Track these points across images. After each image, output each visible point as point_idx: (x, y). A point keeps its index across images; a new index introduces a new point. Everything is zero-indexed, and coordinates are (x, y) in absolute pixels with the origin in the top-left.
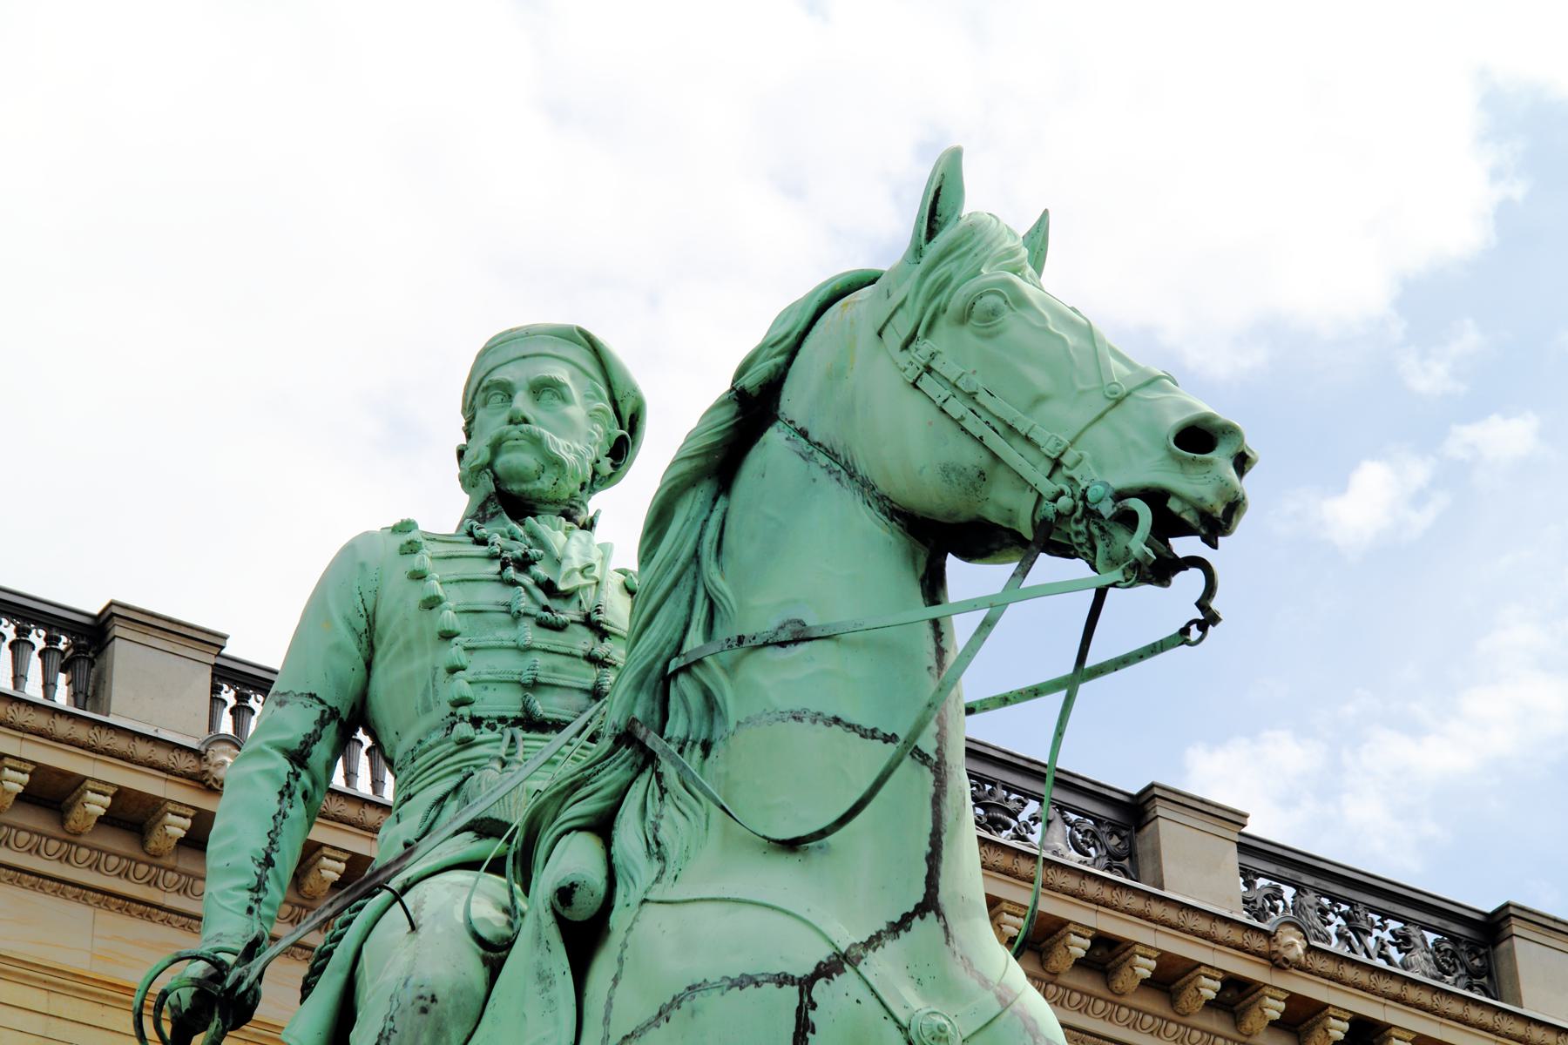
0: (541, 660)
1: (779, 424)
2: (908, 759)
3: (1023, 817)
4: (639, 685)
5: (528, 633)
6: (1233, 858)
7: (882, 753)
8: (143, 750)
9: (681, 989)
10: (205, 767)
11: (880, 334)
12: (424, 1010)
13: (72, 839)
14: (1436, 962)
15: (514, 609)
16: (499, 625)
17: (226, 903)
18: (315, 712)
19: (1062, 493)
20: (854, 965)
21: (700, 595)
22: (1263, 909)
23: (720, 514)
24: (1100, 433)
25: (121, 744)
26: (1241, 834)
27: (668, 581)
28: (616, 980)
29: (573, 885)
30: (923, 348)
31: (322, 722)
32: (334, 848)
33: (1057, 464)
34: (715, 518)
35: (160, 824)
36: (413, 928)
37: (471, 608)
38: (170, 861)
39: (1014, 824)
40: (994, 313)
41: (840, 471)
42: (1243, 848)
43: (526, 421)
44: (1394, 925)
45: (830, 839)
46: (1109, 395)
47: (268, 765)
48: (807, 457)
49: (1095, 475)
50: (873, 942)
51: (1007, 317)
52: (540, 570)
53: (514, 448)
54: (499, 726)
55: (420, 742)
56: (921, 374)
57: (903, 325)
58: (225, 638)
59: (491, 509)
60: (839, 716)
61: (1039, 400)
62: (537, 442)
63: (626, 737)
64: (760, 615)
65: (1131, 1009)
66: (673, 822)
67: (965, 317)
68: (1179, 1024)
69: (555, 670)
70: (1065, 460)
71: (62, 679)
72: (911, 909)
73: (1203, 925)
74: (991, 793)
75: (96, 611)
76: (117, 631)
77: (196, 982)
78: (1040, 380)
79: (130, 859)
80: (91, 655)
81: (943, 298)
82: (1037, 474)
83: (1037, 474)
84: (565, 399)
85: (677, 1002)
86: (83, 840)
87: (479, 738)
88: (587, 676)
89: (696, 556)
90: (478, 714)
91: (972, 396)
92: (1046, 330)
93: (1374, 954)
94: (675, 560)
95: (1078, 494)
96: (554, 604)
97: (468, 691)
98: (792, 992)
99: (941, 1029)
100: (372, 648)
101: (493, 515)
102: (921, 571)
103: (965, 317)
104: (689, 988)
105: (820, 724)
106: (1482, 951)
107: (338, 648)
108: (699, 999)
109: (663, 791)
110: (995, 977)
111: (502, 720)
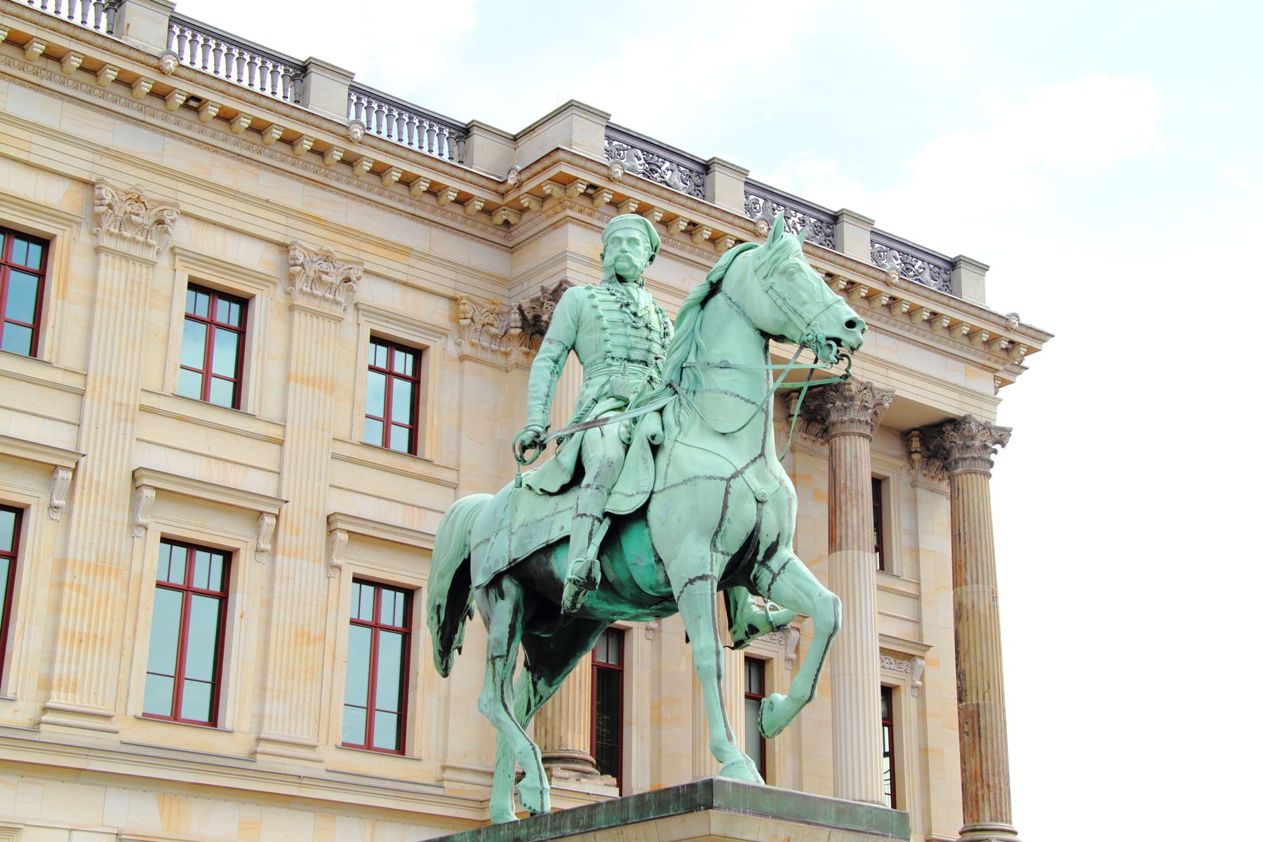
0: (632, 339)
1: (722, 293)
3: (663, 168)
4: (674, 369)
5: (630, 331)
6: (742, 187)
8: (326, 125)
9: (692, 477)
10: (349, 133)
12: (610, 466)
13: (297, 157)
14: (814, 232)
15: (625, 322)
16: (620, 326)
17: (537, 409)
18: (561, 347)
19: (809, 334)
20: (742, 474)
21: (694, 343)
22: (751, 208)
24: (822, 317)
25: (317, 122)
26: (747, 178)
27: (684, 337)
28: (668, 465)
29: (656, 435)
30: (771, 280)
32: (397, 168)
35: (331, 154)
36: (602, 435)
38: (333, 168)
39: (660, 171)
40: (793, 273)
42: (746, 183)
43: (626, 252)
44: (800, 215)
45: (735, 434)
46: (795, 233)
47: (547, 364)
48: (731, 307)
49: (820, 330)
50: (747, 467)
51: (797, 275)
52: (632, 308)
53: (621, 261)
54: (620, 360)
55: (594, 361)
57: (764, 271)
58: (354, 74)
61: (805, 303)
62: (629, 259)
63: (670, 385)
64: (715, 359)
65: (700, 249)
66: (684, 415)
68: (717, 255)
69: (637, 342)
70: (812, 324)
73: (730, 219)
75: (304, 60)
78: (805, 296)
79: (318, 166)
82: (803, 327)
83: (803, 327)
84: (638, 244)
85: (690, 480)
86: (301, 157)
87: (614, 364)
88: (646, 345)
89: (693, 330)
90: (613, 356)
91: (784, 299)
92: (807, 280)
93: (791, 227)
94: (686, 331)
95: (815, 335)
97: (610, 348)
98: (724, 483)
99: (765, 493)
100: (578, 327)
101: (615, 282)
103: (784, 272)
104: (694, 477)
105: (733, 397)
106: (831, 226)
107: (569, 327)
108: (697, 481)
109: (681, 405)
110: (778, 475)
111: (621, 358)
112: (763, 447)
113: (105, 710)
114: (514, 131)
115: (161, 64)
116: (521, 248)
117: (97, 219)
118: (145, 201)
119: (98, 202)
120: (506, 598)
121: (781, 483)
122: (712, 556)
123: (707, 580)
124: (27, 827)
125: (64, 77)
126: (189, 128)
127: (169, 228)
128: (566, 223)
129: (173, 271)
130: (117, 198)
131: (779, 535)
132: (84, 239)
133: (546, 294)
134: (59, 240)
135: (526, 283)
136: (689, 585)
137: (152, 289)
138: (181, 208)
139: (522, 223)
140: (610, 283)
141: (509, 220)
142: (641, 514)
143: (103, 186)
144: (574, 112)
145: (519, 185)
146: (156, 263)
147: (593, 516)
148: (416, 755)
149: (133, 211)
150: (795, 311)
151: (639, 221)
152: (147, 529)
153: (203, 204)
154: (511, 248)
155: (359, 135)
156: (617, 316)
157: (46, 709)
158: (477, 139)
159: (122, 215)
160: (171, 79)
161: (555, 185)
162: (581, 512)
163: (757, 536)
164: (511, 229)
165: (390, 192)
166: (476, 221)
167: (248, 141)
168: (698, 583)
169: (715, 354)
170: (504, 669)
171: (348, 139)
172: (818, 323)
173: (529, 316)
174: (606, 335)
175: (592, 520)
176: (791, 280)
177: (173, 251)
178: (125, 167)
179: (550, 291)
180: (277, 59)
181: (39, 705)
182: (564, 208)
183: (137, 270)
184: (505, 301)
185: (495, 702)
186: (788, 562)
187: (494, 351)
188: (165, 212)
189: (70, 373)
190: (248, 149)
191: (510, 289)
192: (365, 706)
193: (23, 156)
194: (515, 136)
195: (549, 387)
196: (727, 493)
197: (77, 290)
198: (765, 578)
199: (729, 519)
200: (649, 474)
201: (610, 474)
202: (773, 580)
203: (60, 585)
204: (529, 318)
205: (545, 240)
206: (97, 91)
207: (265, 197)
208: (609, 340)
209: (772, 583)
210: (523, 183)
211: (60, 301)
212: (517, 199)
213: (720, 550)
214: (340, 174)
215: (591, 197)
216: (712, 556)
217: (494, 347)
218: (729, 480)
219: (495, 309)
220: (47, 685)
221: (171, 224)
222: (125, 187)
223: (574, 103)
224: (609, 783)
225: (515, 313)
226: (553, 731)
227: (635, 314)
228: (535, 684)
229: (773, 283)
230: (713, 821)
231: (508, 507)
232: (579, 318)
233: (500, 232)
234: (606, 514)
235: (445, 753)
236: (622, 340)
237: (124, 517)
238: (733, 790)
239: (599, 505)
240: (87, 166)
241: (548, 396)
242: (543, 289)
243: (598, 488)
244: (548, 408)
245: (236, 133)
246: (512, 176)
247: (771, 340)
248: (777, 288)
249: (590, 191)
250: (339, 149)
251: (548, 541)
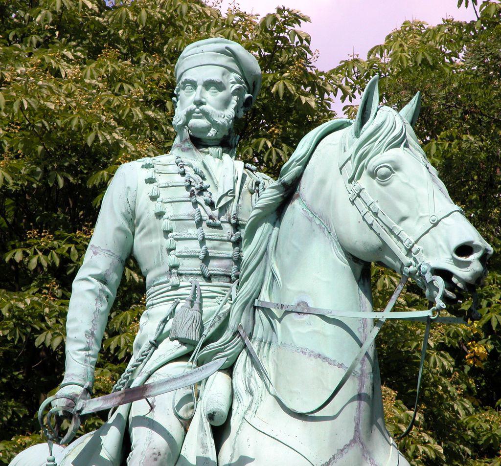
1: (300, 199)
11: (341, 169)
12: (156, 459)
17: (75, 357)
23: (276, 232)
37: (177, 218)
41: (324, 228)
56: (356, 198)
60: (321, 354)
61: (404, 219)
64: (291, 301)
78: (404, 209)
81: (365, 161)
82: (401, 253)
87: (182, 284)
89: (266, 251)
94: (257, 252)
105: (312, 358)
107: (120, 229)
114: (150, 408)
150: (391, 231)
208: (174, 249)
232: (133, 213)
236: (194, 246)
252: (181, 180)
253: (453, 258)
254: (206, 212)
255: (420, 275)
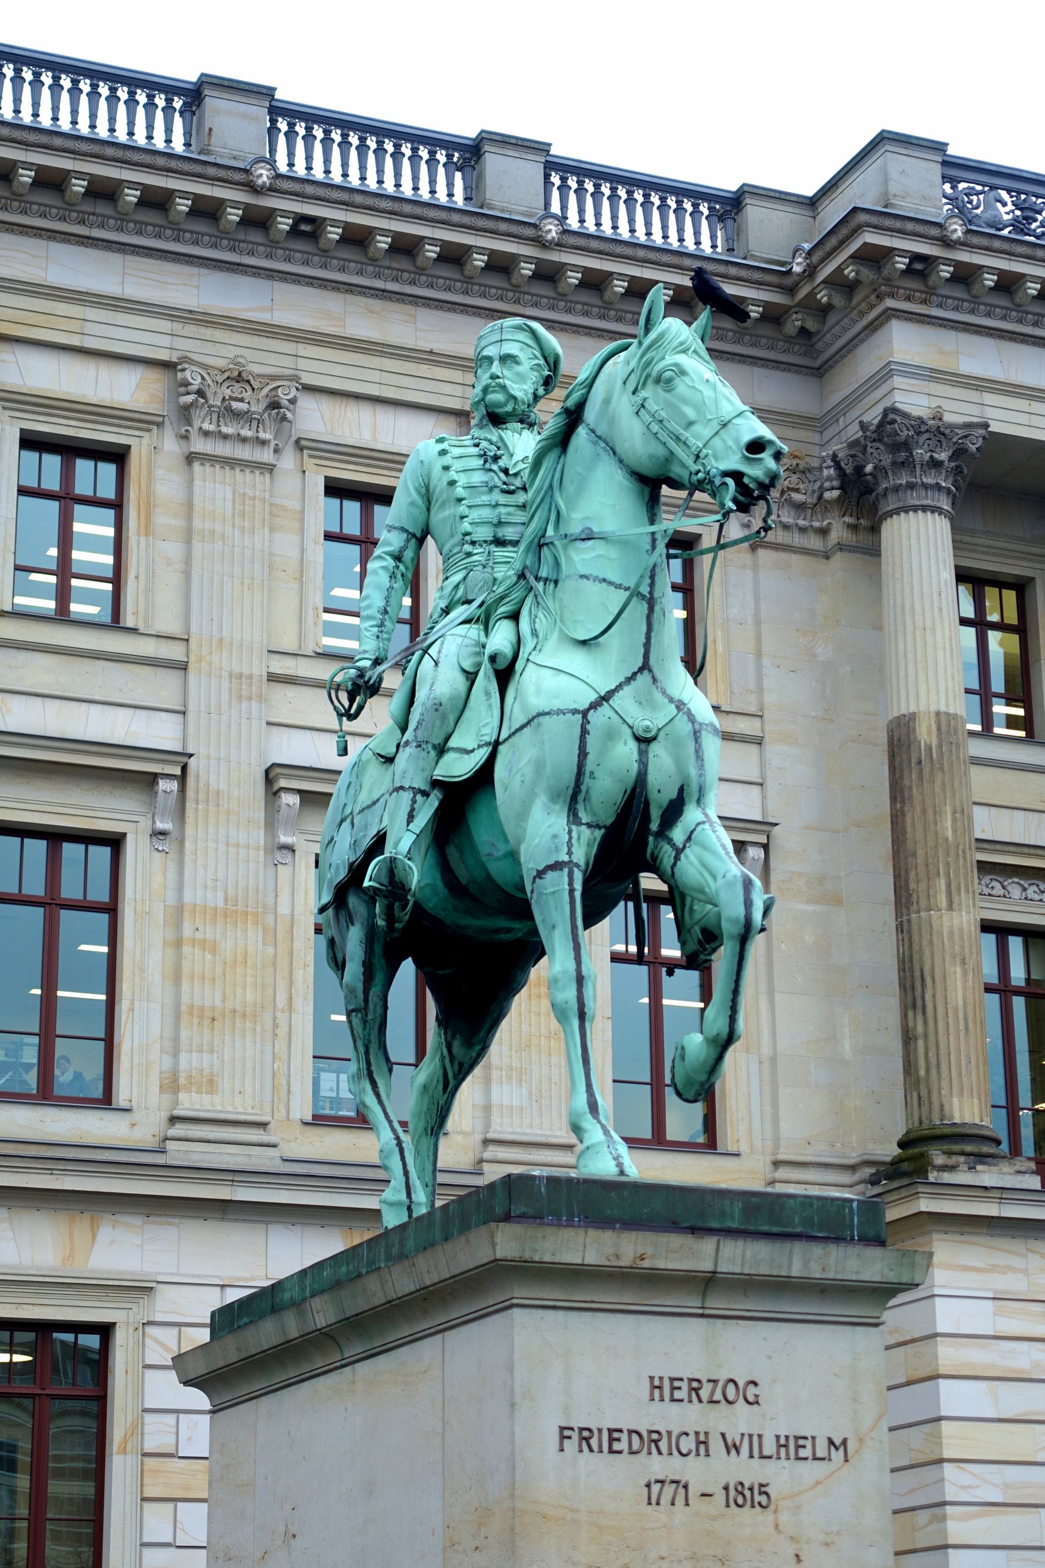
0: (503, 510)
2: (635, 599)
7: (624, 595)
8: (503, 227)
11: (624, 383)
12: (437, 710)
16: (483, 493)
17: (367, 634)
19: (699, 471)
24: (717, 442)
30: (643, 394)
31: (408, 541)
33: (698, 457)
34: (560, 467)
40: (670, 380)
43: (498, 377)
45: (600, 639)
47: (384, 564)
48: (595, 443)
49: (713, 462)
50: (619, 687)
59: (484, 422)
61: (690, 424)
62: (504, 387)
64: (575, 527)
67: (658, 381)
70: (702, 455)
71: (458, 175)
72: (636, 670)
74: (1024, 200)
76: (486, 148)
77: (351, 679)
78: (690, 413)
80: (473, 163)
82: (689, 462)
83: (689, 462)
84: (518, 363)
85: (533, 718)
86: (474, 281)
87: (475, 551)
89: (551, 486)
92: (694, 387)
96: (511, 480)
99: (647, 727)
102: (647, 499)
103: (658, 381)
109: (538, 603)
111: (485, 542)
112: (646, 656)
113: (256, 1114)
114: (810, 191)
115: (251, 178)
116: (831, 367)
117: (185, 413)
118: (251, 378)
119: (182, 389)
120: (355, 922)
121: (678, 708)
122: (570, 832)
123: (561, 870)
124: (160, 1286)
125: (121, 219)
126: (306, 263)
127: (287, 412)
128: (888, 319)
129: (300, 475)
130: (209, 381)
131: (681, 790)
132: (170, 444)
133: (868, 434)
134: (134, 451)
135: (841, 420)
136: (537, 880)
137: (271, 505)
138: (302, 381)
139: (826, 327)
140: (481, 428)
141: (807, 327)
142: (485, 775)
143: (186, 366)
144: (888, 147)
145: (811, 272)
146: (274, 466)
147: (414, 788)
148: (732, 1148)
149: (234, 395)
150: (678, 439)
151: (519, 328)
152: (294, 851)
153: (338, 370)
154: (819, 369)
155: (554, 234)
156: (478, 478)
157: (174, 1120)
158: (754, 212)
159: (219, 404)
160: (269, 198)
161: (862, 265)
162: (397, 784)
163: (641, 793)
164: (813, 341)
165: (617, 310)
166: (757, 336)
167: (393, 269)
168: (550, 875)
169: (575, 523)
170: (364, 1029)
171: (539, 242)
172: (710, 452)
173: (849, 470)
174: (462, 509)
175: (412, 795)
176: (669, 391)
177: (299, 446)
178: (219, 335)
179: (873, 428)
180: (434, 141)
181: (164, 1115)
182: (880, 298)
183: (253, 483)
184: (816, 451)
185: (359, 1078)
186: (694, 829)
187: (802, 530)
188: (280, 390)
189: (165, 640)
190: (396, 279)
191: (821, 432)
192: (648, 1080)
193: (75, 341)
194: (811, 198)
195: (387, 599)
196: (584, 732)
197: (166, 520)
198: (667, 854)
199: (592, 773)
200: (492, 716)
201: (438, 723)
202: (677, 858)
203: (178, 943)
204: (848, 471)
205: (862, 350)
206: (169, 232)
207: (427, 347)
208: (467, 517)
209: (675, 864)
210: (815, 267)
211: (143, 539)
212: (812, 294)
213: (584, 821)
214: (537, 295)
215: (922, 275)
216: (570, 832)
217: (801, 522)
218: (585, 714)
219: (797, 465)
220: (172, 1084)
221: (291, 407)
222: (221, 363)
223: (885, 135)
224: (1022, 1169)
225: (828, 467)
226: (929, 1097)
227: (506, 471)
228: (449, 1047)
229: (645, 400)
230: (498, 1239)
231: (352, 786)
233: (796, 348)
234: (436, 784)
235: (777, 1140)
236: (486, 513)
237: (259, 836)
238: (547, 1189)
239: (423, 770)
240: (165, 341)
241: (386, 612)
242: (863, 426)
243: (419, 746)
244: (385, 630)
245: (374, 260)
246: (799, 260)
247: (664, 486)
248: (652, 406)
249: (918, 266)
250: (528, 259)
251: (379, 832)
252: (475, 451)
253: (744, 456)
254: (498, 479)
255: (710, 480)
